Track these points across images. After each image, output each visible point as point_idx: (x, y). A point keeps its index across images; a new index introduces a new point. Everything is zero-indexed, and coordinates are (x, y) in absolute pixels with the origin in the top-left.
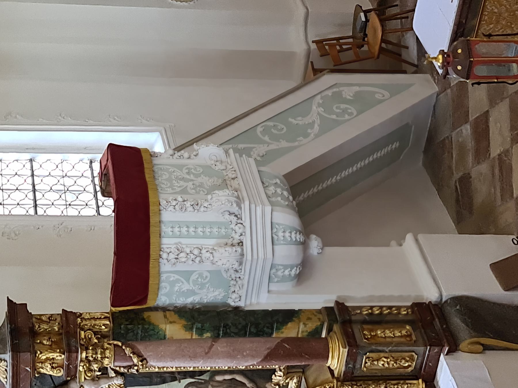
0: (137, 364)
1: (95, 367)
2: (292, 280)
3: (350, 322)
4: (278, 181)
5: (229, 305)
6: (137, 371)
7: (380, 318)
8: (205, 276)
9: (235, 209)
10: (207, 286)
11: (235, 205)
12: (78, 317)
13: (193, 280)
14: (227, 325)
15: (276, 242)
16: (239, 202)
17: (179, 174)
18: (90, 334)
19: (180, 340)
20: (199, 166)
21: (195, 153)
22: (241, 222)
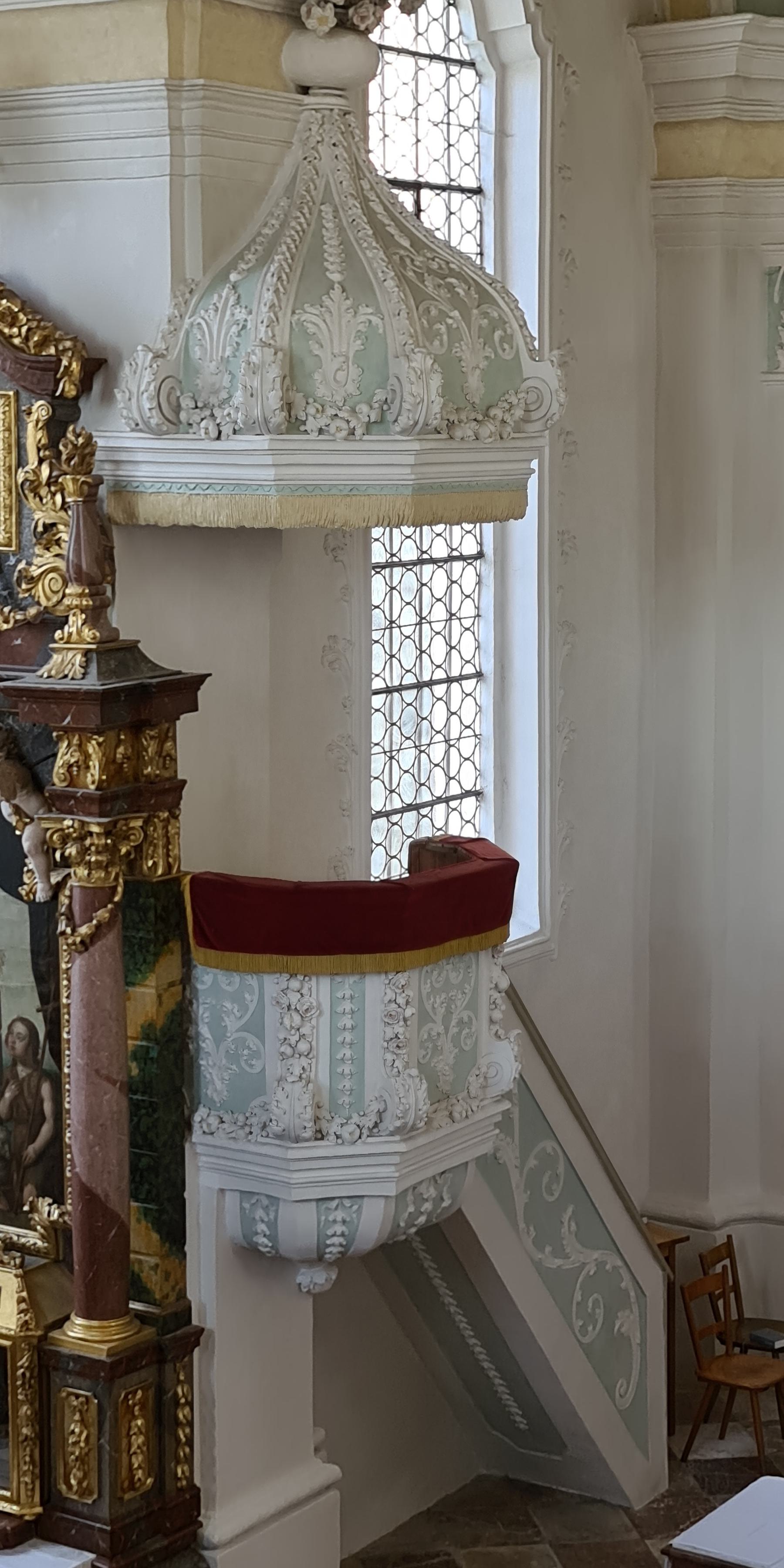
0: (76, 934)
1: (72, 850)
2: (244, 1237)
3: (161, 1362)
4: (445, 1204)
5: (193, 1111)
6: (63, 933)
7: (168, 1423)
8: (253, 1062)
9: (390, 1123)
10: (234, 1067)
11: (398, 1123)
12: (170, 811)
13: (244, 1040)
14: (154, 1111)
15: (324, 1206)
16: (406, 1131)
17: (459, 1003)
18: (137, 837)
19: (125, 1018)
20: (476, 1043)
21: (501, 1032)
22: (364, 1136)
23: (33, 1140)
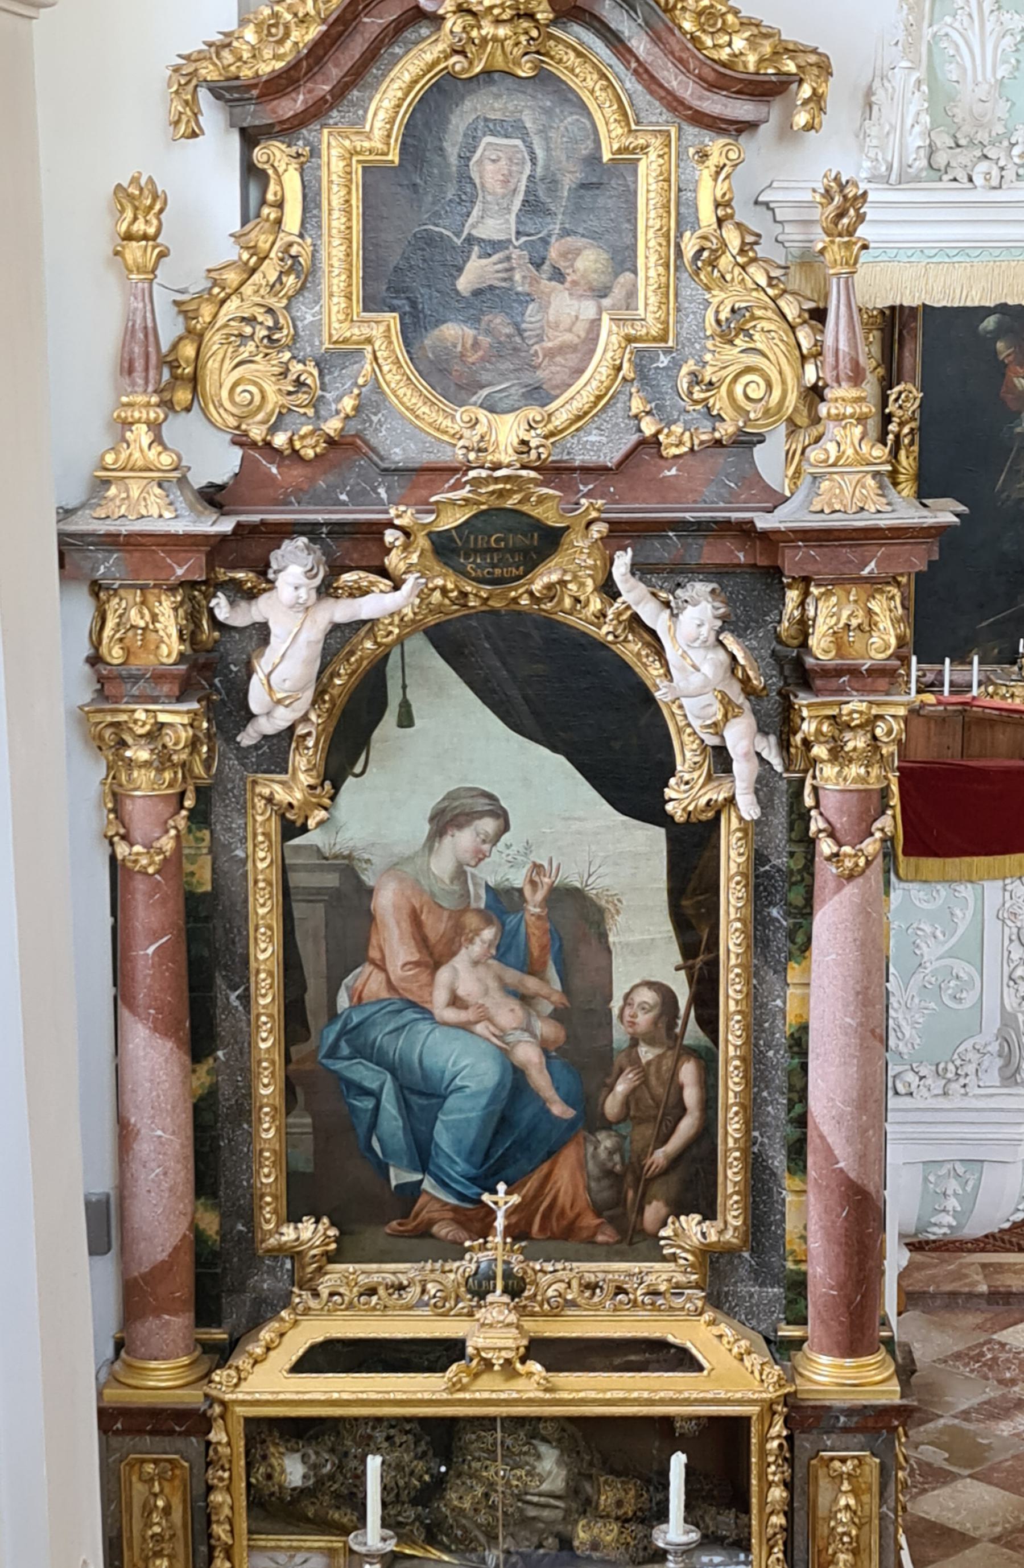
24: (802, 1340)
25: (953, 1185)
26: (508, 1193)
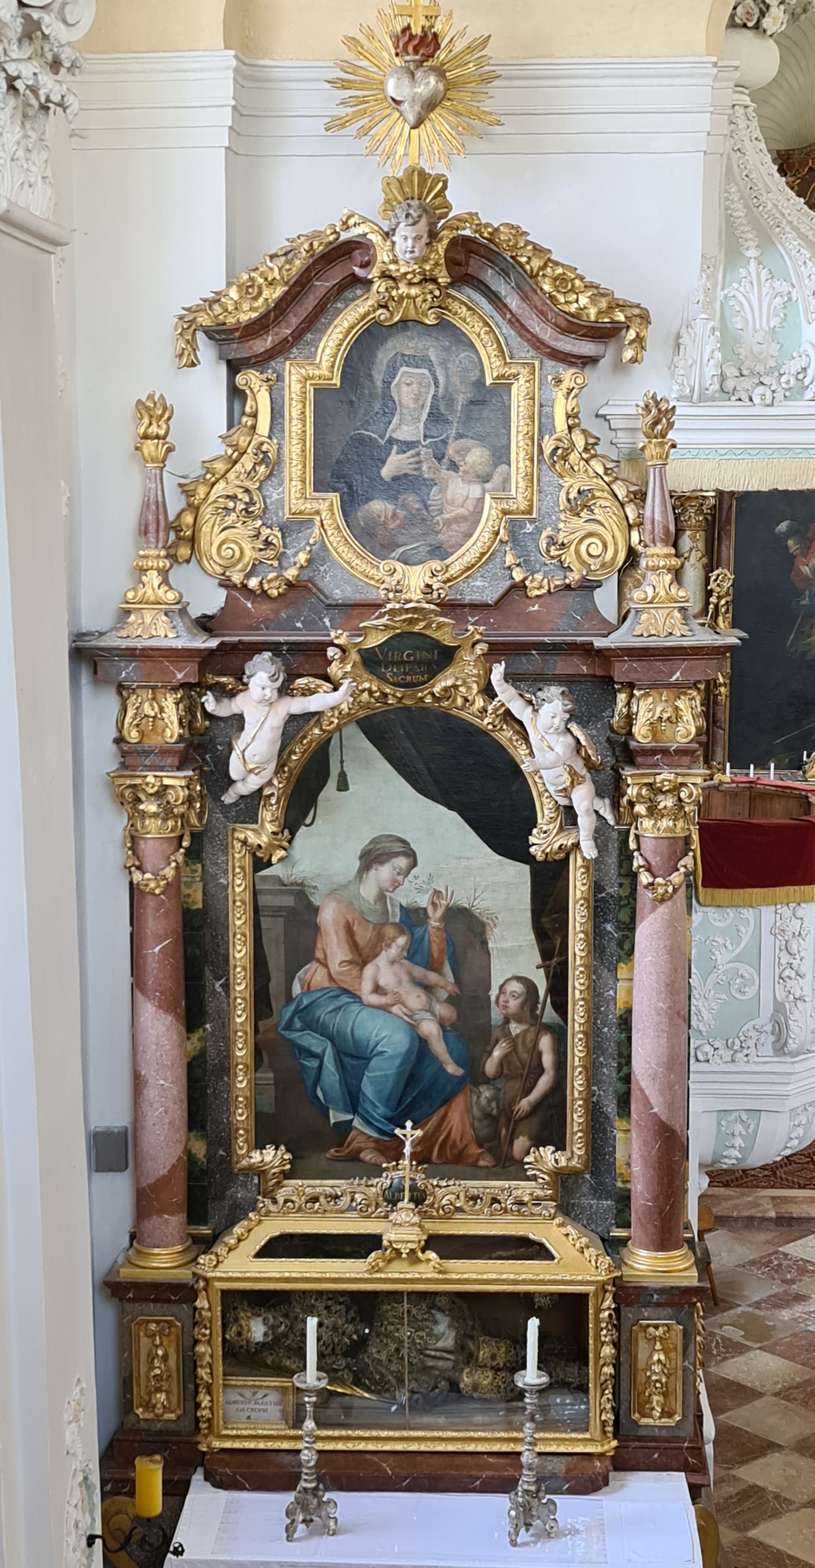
10: (724, 996)
23: (527, 1092)
24: (628, 1239)
25: (739, 1128)
26: (413, 1128)
